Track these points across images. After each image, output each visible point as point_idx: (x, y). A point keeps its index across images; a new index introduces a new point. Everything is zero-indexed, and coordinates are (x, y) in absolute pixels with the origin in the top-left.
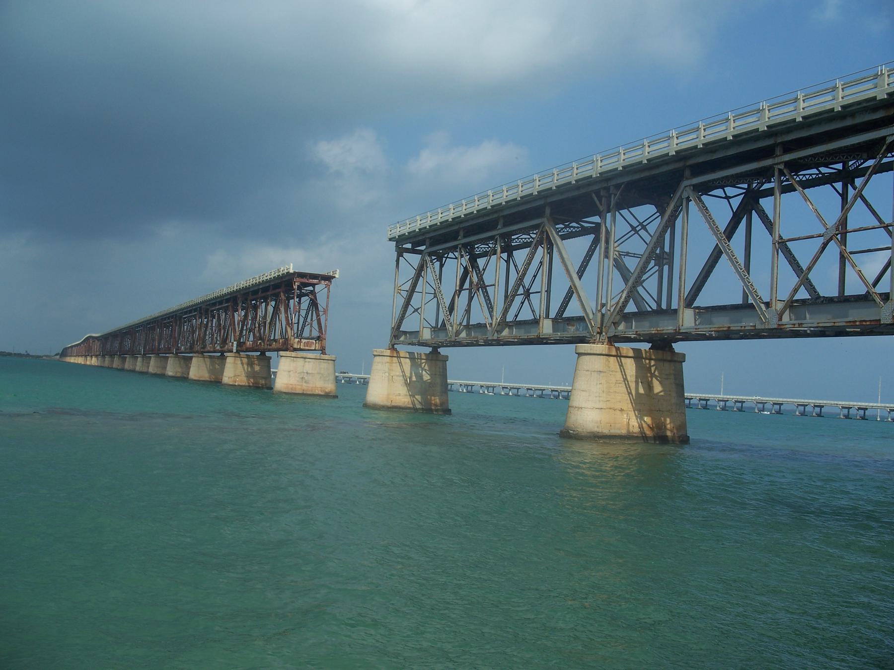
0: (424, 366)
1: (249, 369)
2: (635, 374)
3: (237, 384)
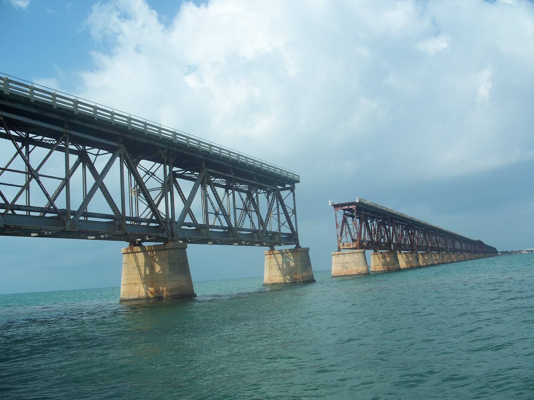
0: (290, 257)
1: (384, 261)
2: (144, 261)
3: (377, 270)
